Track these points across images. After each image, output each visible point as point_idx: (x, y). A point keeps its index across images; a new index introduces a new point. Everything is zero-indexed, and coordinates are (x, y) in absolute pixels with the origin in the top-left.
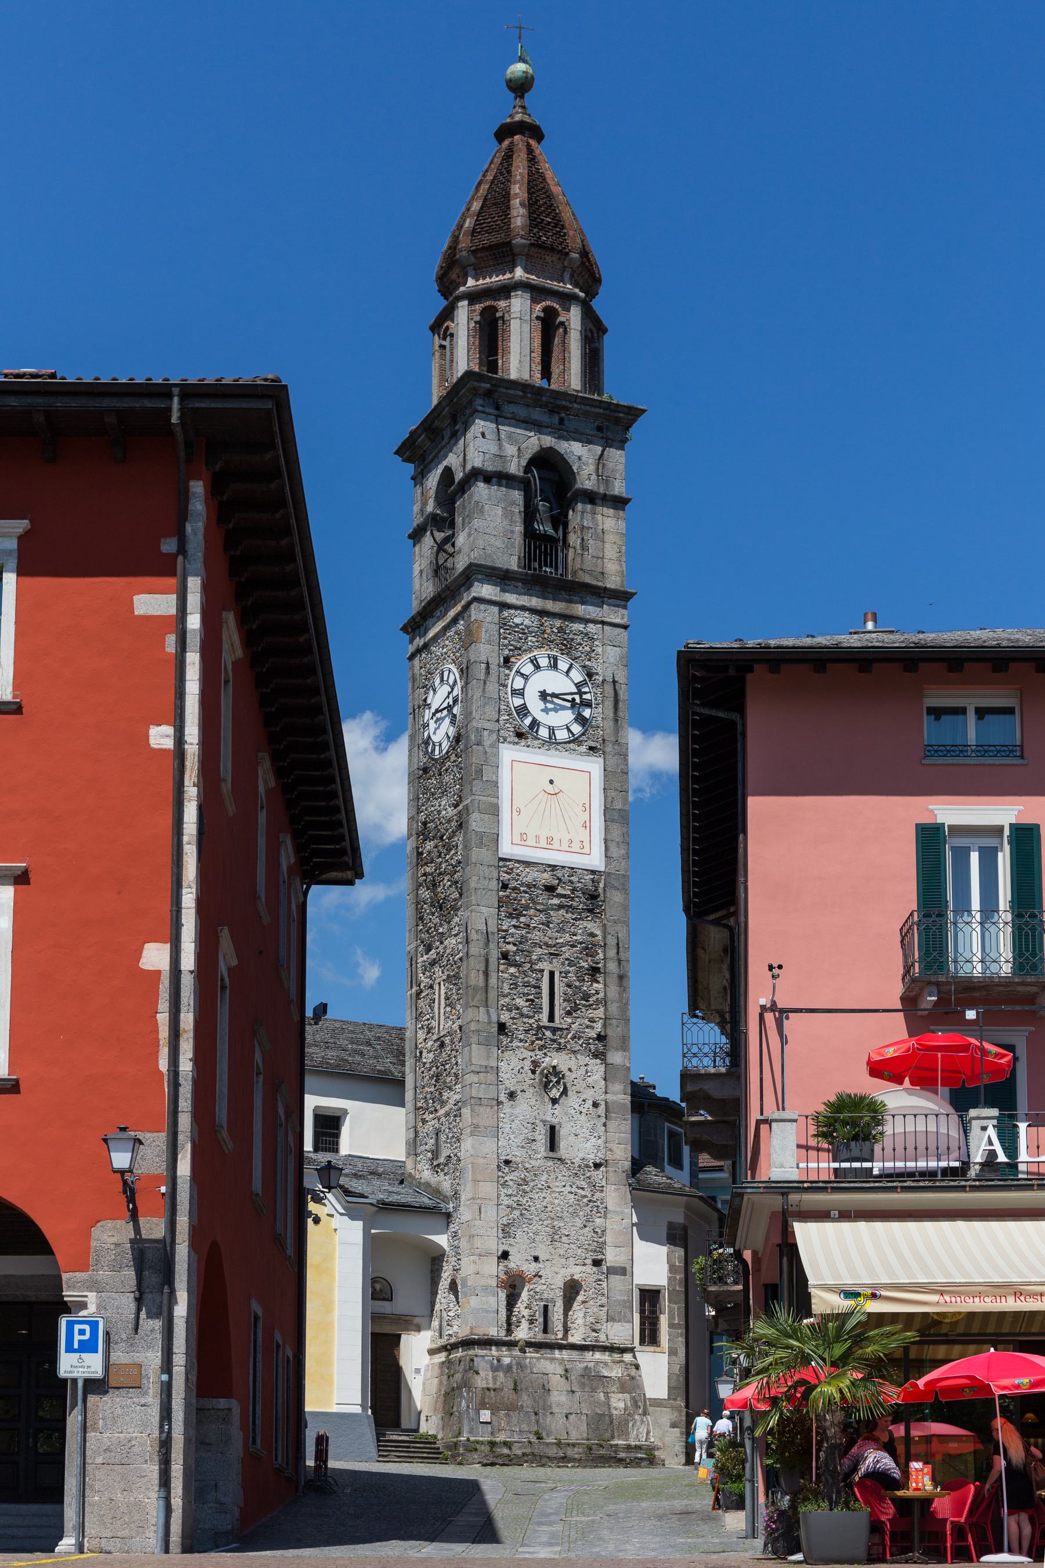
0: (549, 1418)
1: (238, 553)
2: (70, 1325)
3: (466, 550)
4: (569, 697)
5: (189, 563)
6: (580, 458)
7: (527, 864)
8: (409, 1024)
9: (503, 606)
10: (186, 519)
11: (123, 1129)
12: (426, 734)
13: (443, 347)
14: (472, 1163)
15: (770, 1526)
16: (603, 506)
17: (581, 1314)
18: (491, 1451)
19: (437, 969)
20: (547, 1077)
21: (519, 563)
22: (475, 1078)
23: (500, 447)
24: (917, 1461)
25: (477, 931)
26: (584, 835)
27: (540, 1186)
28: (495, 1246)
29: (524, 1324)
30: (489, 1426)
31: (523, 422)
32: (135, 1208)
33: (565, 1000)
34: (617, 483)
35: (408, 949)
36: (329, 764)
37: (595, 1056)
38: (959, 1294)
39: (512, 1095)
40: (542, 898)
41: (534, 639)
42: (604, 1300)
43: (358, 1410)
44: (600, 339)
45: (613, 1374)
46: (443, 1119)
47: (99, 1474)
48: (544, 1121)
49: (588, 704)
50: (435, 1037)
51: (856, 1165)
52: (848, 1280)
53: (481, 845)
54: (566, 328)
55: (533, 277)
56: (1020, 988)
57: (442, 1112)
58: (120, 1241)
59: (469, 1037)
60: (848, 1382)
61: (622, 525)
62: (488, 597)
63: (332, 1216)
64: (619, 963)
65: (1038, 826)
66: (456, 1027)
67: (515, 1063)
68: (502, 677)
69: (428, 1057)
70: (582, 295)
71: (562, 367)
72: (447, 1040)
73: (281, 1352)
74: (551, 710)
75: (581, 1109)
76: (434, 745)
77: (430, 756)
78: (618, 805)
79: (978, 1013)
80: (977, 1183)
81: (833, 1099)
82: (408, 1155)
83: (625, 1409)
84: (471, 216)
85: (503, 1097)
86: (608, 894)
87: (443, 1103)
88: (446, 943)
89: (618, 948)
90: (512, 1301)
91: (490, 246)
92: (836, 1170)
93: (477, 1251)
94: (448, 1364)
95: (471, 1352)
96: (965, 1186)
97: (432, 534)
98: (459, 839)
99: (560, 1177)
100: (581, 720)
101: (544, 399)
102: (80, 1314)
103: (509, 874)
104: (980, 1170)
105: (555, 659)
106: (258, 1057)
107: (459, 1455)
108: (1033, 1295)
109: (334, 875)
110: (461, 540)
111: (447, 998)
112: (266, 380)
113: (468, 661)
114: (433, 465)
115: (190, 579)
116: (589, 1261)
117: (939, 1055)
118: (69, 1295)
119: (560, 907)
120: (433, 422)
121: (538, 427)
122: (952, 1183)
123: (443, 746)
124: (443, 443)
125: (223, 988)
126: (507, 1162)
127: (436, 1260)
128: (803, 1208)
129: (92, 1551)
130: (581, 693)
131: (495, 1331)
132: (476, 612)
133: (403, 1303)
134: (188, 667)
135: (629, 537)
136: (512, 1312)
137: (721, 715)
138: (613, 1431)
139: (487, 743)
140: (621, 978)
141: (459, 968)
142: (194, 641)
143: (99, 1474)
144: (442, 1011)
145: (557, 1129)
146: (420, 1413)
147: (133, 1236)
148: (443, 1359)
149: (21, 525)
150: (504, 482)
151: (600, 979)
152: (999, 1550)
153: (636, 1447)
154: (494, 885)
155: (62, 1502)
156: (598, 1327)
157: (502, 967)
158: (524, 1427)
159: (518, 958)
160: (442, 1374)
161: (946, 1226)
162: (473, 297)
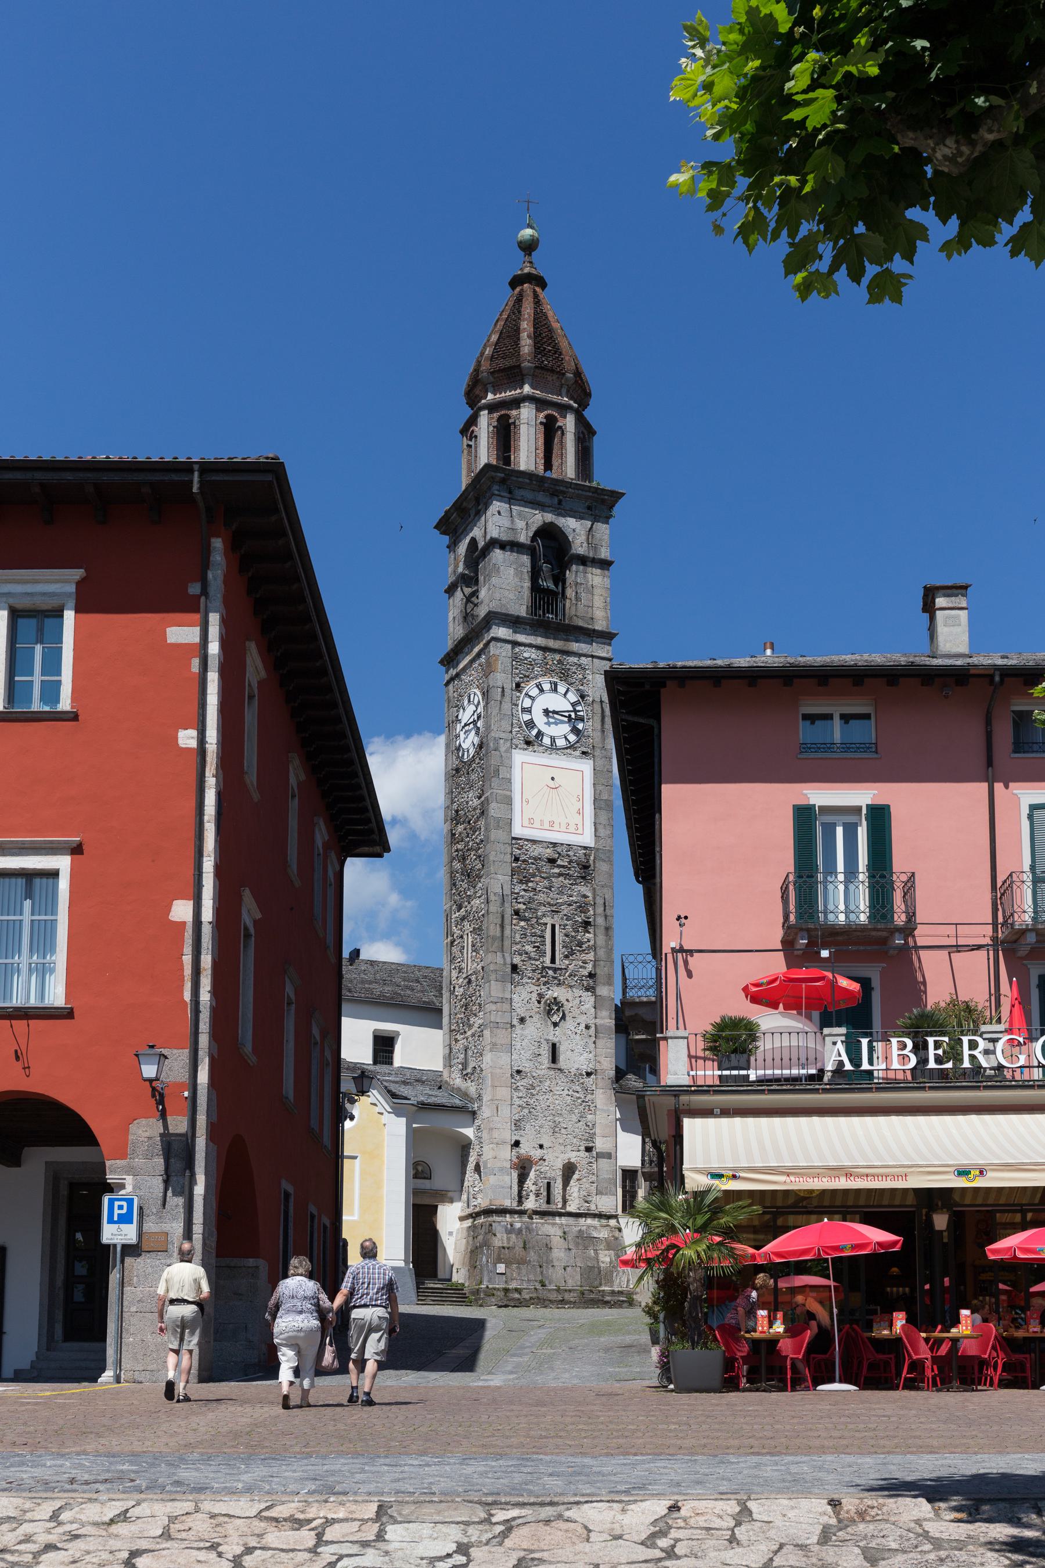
0: (551, 1270)
1: (258, 596)
2: (111, 1203)
3: (486, 601)
4: (567, 714)
5: (210, 602)
6: (574, 531)
7: (534, 842)
8: (445, 966)
9: (515, 644)
10: (208, 568)
11: (152, 1047)
12: (458, 742)
13: (469, 446)
14: (491, 1073)
15: (663, 1360)
16: (592, 567)
17: (576, 1189)
18: (505, 1295)
19: (466, 923)
20: (549, 1006)
21: (527, 611)
22: (493, 1007)
23: (513, 522)
24: (763, 1309)
25: (495, 894)
26: (578, 819)
27: (544, 1090)
28: (510, 1137)
29: (532, 1197)
30: (504, 1278)
31: (530, 503)
32: (164, 1109)
33: (563, 947)
34: (603, 550)
35: (445, 908)
36: (351, 763)
37: (587, 990)
38: (802, 1175)
39: (522, 1020)
40: (546, 868)
41: (539, 669)
42: (594, 1178)
43: (402, 1264)
44: (590, 439)
45: (601, 1236)
46: (470, 1039)
47: (134, 1320)
48: (547, 1040)
49: (582, 719)
50: (464, 976)
51: (735, 1072)
52: (715, 1165)
53: (498, 827)
54: (563, 431)
55: (538, 392)
56: (874, 933)
57: (469, 1033)
58: (152, 1135)
59: (489, 975)
60: (704, 1247)
61: (607, 581)
62: (503, 637)
63: (382, 1114)
64: (606, 918)
65: (889, 806)
66: (479, 967)
67: (525, 995)
68: (514, 698)
69: (459, 991)
70: (575, 405)
71: (560, 461)
72: (473, 978)
73: (316, 1221)
74: (553, 723)
75: (576, 1030)
76: (463, 751)
77: (460, 759)
78: (605, 797)
79: (830, 952)
80: (828, 1087)
81: (718, 1020)
82: (445, 1066)
83: (611, 1263)
84: (490, 346)
85: (515, 1022)
86: (597, 865)
87: (470, 1026)
88: (472, 903)
89: (605, 906)
90: (522, 1179)
91: (504, 369)
92: (720, 1076)
93: (495, 1141)
94: (473, 1228)
95: (490, 1219)
96: (818, 1089)
97: (462, 589)
98: (482, 823)
99: (560, 1083)
100: (575, 731)
101: (546, 485)
102: (120, 1193)
103: (520, 849)
104: (832, 1076)
105: (556, 685)
106: (289, 990)
107: (480, 1299)
108: (861, 1176)
109: (366, 849)
110: (483, 593)
111: (473, 946)
112: (267, 458)
113: (488, 686)
114: (462, 536)
115: (211, 615)
116: (582, 1148)
117: (804, 985)
118: (111, 1178)
119: (560, 875)
120: (462, 504)
121: (541, 507)
122: (809, 1087)
123: (470, 751)
124: (470, 520)
125: (247, 936)
126: (519, 1072)
127: (464, 1147)
128: (692, 1107)
129: (127, 1382)
130: (575, 711)
131: (509, 1203)
132: (493, 649)
133: (441, 1180)
134: (209, 684)
135: (613, 591)
136: (523, 1187)
137: (641, 721)
138: (601, 1279)
139: (503, 749)
140: (607, 929)
141: (482, 922)
142: (214, 664)
143: (134, 1320)
144: (470, 955)
145: (557, 1046)
146: (452, 1266)
147: (162, 1131)
148: (470, 1224)
149: (78, 574)
150: (515, 548)
151: (591, 930)
152: (831, 1380)
153: (619, 1291)
154: (508, 858)
155: (105, 1341)
156: (590, 1199)
157: (514, 922)
158: (532, 1277)
159: (527, 914)
160: (469, 1236)
161: (882, 1120)
162: (492, 408)
